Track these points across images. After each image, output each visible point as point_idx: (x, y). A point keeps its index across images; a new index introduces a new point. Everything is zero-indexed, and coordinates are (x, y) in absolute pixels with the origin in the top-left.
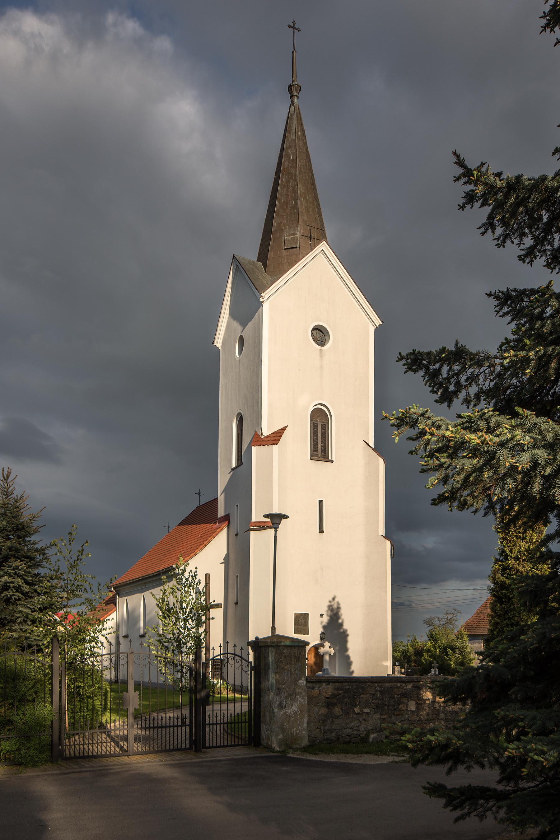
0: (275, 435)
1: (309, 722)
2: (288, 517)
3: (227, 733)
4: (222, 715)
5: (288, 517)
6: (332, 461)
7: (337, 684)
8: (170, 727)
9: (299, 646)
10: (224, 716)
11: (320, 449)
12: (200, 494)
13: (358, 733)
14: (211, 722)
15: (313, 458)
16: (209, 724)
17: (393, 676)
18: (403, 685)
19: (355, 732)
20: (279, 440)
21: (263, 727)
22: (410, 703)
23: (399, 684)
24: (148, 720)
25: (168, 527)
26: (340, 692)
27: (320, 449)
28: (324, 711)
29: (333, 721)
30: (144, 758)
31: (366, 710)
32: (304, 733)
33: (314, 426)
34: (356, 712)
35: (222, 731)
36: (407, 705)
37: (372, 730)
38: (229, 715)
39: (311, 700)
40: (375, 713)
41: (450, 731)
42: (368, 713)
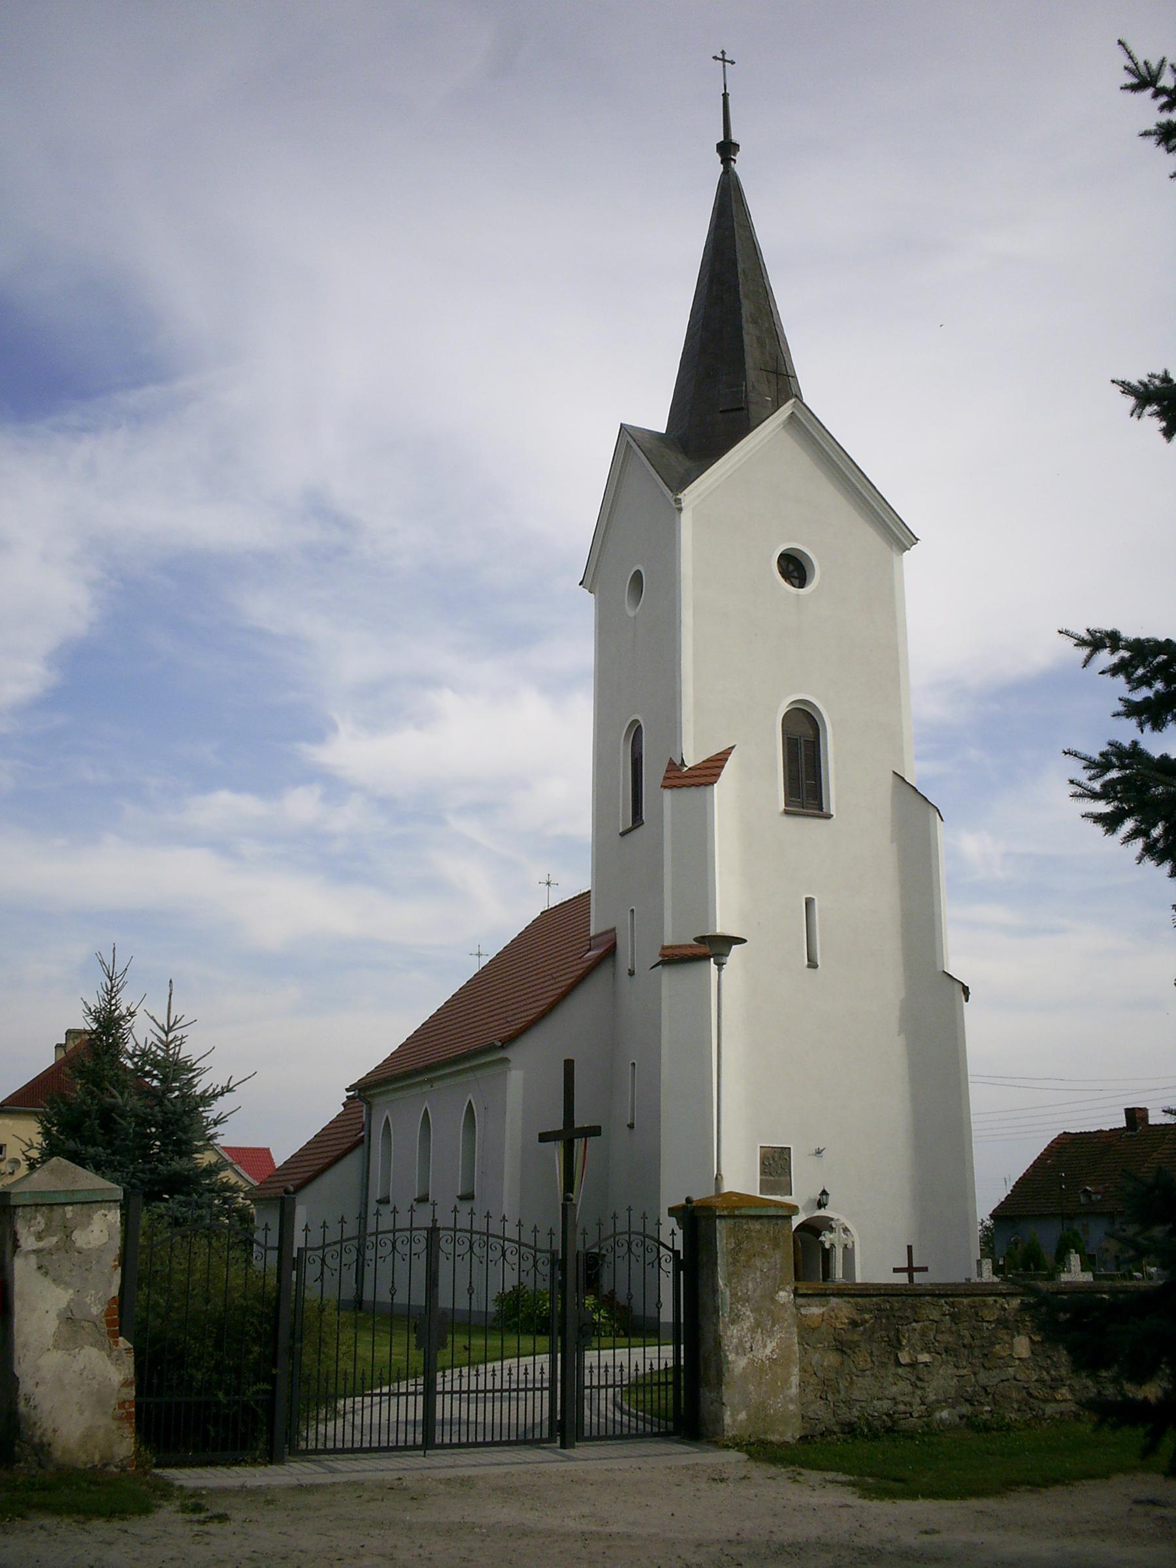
1: (803, 1385)
2: (745, 941)
3: (621, 1409)
4: (359, 1376)
5: (745, 941)
6: (829, 817)
7: (859, 1299)
8: (452, 1392)
9: (778, 1217)
10: (363, 1379)
11: (805, 787)
12: (548, 883)
13: (908, 1409)
15: (669, 782)
16: (444, 1393)
17: (978, 1280)
18: (1001, 1300)
19: (901, 1407)
20: (718, 775)
21: (706, 1395)
22: (1017, 1339)
23: (991, 1299)
24: (498, 1373)
25: (479, 955)
26: (867, 1316)
27: (805, 787)
28: (832, 1359)
30: (209, 1476)
31: (924, 1358)
32: (791, 1407)
33: (791, 745)
34: (903, 1362)
35: (610, 1407)
36: (1012, 1346)
37: (938, 1401)
39: (807, 1332)
40: (945, 1363)
41: (831, 1416)
42: (926, 1364)
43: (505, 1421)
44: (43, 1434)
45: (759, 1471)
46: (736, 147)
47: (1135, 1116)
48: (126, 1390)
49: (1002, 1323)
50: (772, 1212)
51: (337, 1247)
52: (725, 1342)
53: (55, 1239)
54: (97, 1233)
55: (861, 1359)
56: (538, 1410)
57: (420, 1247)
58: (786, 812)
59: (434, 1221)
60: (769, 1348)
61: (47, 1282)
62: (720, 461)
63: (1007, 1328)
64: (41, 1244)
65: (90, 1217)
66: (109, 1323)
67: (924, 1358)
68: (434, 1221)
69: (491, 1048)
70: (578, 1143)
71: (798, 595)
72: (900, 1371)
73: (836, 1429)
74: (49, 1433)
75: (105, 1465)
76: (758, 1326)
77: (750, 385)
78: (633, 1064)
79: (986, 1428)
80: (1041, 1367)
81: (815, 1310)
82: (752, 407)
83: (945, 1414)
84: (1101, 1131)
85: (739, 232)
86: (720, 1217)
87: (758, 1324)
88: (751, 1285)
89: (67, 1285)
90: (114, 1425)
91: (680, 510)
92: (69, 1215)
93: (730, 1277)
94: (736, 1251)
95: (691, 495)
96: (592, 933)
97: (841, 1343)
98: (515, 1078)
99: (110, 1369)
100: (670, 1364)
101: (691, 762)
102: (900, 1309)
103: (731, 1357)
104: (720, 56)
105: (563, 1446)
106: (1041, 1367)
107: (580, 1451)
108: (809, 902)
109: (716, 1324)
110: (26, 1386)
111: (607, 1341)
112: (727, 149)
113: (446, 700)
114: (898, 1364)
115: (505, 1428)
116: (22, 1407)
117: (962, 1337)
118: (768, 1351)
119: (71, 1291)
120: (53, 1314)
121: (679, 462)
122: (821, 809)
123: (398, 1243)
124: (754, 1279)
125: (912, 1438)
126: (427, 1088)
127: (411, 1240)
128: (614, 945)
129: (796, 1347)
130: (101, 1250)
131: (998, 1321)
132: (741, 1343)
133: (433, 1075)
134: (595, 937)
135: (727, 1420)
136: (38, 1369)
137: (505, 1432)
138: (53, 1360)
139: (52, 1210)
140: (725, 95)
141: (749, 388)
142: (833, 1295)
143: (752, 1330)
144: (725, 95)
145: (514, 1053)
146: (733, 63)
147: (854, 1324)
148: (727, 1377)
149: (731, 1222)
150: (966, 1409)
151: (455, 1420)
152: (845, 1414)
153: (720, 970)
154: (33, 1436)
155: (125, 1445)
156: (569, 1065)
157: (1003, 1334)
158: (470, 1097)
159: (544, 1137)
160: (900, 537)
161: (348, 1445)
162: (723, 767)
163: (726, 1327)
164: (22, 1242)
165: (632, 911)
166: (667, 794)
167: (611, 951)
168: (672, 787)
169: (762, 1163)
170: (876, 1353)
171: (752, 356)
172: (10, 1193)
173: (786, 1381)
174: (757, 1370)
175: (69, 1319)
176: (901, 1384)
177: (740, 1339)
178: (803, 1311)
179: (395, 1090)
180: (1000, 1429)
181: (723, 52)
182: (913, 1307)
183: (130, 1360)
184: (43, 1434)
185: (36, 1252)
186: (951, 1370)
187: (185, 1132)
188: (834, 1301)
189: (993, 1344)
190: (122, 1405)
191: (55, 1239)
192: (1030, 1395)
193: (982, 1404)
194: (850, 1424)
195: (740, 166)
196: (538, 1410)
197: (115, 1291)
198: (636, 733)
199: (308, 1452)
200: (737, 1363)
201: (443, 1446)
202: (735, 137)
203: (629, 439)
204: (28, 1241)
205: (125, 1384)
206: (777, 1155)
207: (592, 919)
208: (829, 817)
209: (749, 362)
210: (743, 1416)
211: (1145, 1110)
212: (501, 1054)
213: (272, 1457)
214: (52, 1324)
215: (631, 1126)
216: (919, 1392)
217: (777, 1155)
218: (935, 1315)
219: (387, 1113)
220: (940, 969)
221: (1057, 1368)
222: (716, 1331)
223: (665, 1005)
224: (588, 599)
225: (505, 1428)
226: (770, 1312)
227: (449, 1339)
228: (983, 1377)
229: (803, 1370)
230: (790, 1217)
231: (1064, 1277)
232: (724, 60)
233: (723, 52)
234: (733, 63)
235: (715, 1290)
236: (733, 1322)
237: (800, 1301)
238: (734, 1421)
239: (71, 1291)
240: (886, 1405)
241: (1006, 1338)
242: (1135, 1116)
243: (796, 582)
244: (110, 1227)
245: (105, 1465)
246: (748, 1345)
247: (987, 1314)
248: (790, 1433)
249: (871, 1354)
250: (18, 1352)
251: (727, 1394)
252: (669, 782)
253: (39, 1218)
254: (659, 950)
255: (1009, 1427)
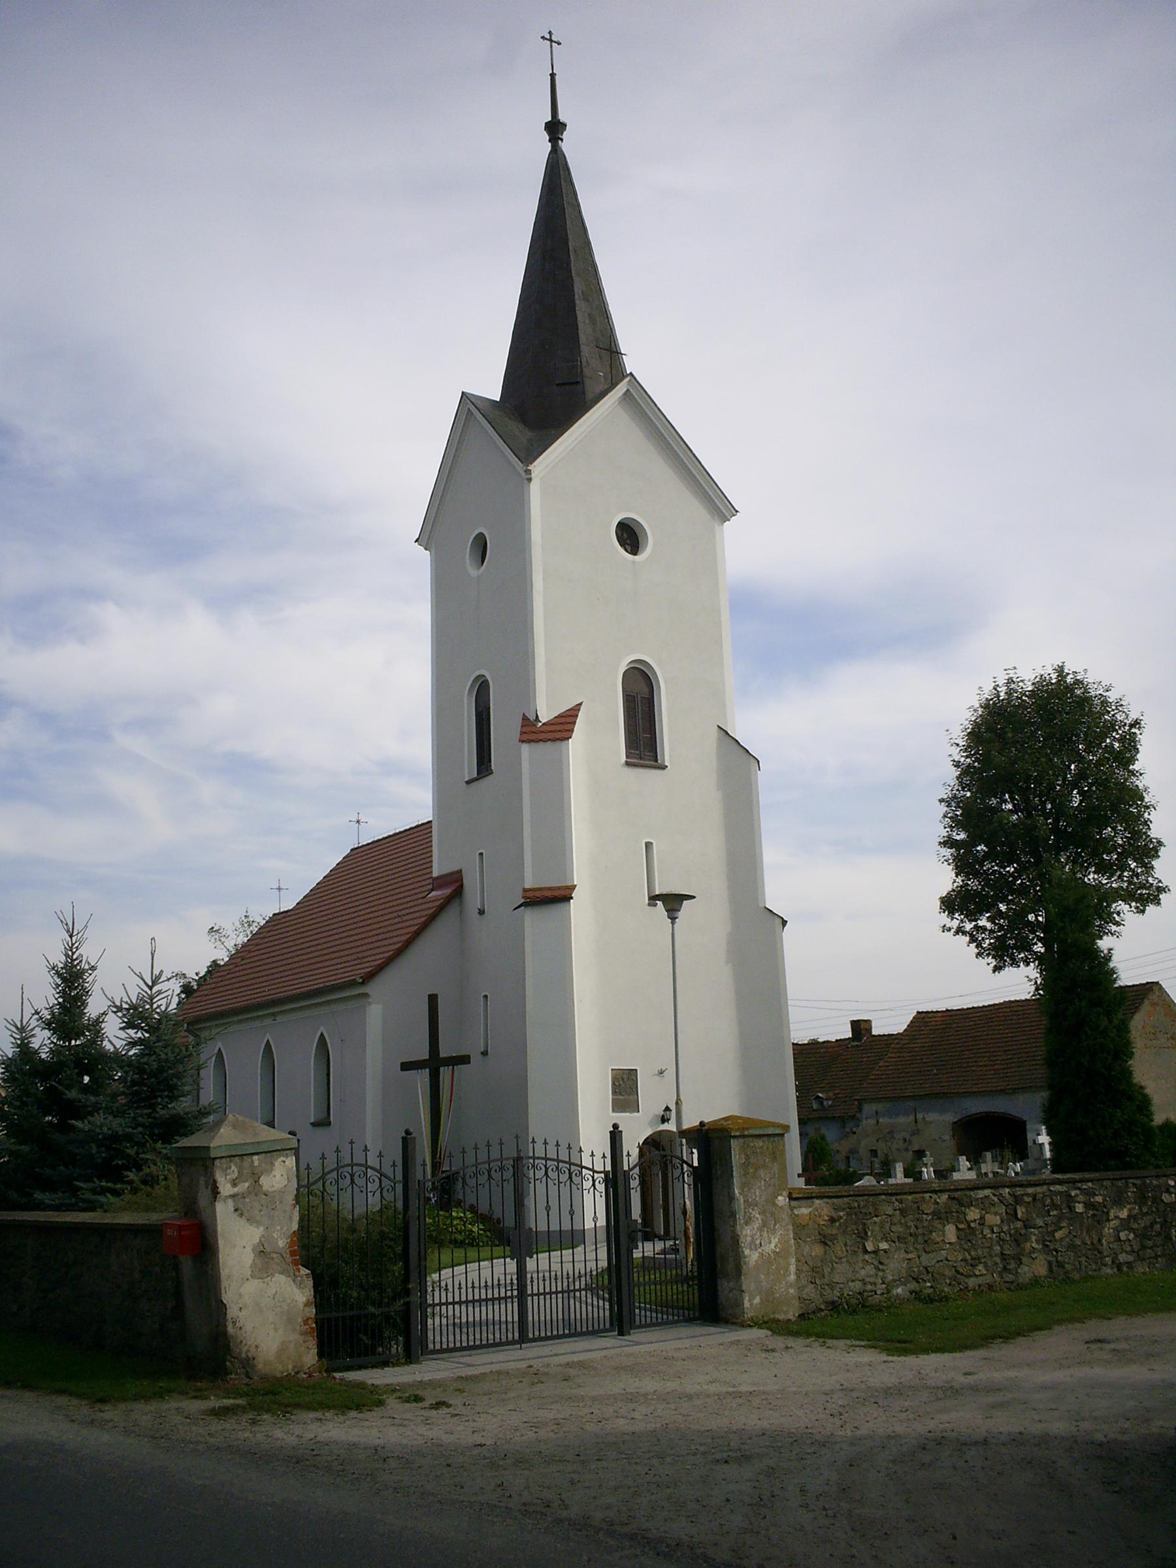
0: (563, 720)
1: (799, 1271)
6: (664, 767)
11: (643, 744)
14: (535, 1291)
15: (526, 737)
16: (532, 1295)
18: (934, 1196)
19: (869, 1287)
21: (724, 1286)
23: (927, 1195)
27: (643, 744)
28: (818, 1250)
29: (833, 1269)
31: (884, 1246)
32: (791, 1291)
33: (630, 701)
37: (894, 1281)
38: (565, 1273)
39: (800, 1229)
42: (885, 1251)
43: (578, 1317)
44: (248, 1351)
45: (779, 1342)
46: (564, 126)
47: (860, 1028)
48: (307, 1309)
49: (936, 1215)
50: (770, 1131)
51: (334, 1174)
52: (742, 1240)
53: (247, 1185)
54: (278, 1177)
55: (839, 1249)
56: (554, 1310)
57: (508, 1174)
58: (627, 764)
59: (519, 1151)
60: (772, 1244)
61: (242, 1222)
62: (565, 435)
63: (939, 1218)
64: (236, 1190)
65: (273, 1164)
66: (292, 1253)
67: (884, 1246)
68: (519, 1151)
69: (352, 984)
70: (445, 1072)
71: (634, 562)
72: (867, 1257)
73: (823, 1307)
74: (253, 1350)
75: (297, 1373)
76: (764, 1226)
77: (584, 360)
78: (486, 997)
79: (930, 1300)
80: (965, 1250)
81: (804, 1211)
82: (587, 382)
83: (899, 1290)
84: (828, 1042)
85: (568, 211)
86: (735, 1137)
87: (764, 1224)
88: (758, 1193)
89: (258, 1223)
90: (301, 1339)
91: (530, 480)
92: (256, 1163)
93: (743, 1186)
94: (745, 1166)
95: (541, 466)
96: (435, 874)
97: (824, 1236)
98: (375, 1013)
99: (294, 1293)
100: (605, 1264)
101: (544, 719)
102: (865, 1206)
103: (747, 1252)
104: (548, 36)
105: (621, 1333)
106: (965, 1250)
107: (636, 1336)
108: (648, 845)
109: (734, 1226)
110: (232, 1312)
111: (486, 1251)
112: (555, 129)
113: (109, 614)
114: (866, 1251)
115: (602, 1320)
116: (230, 1329)
117: (909, 1228)
118: (772, 1246)
119: (262, 1228)
120: (249, 1249)
121: (523, 434)
122: (656, 761)
123: (493, 1172)
124: (760, 1188)
125: (880, 1310)
126: (268, 1021)
127: (502, 1168)
128: (462, 886)
129: (793, 1241)
130: (282, 1192)
131: (933, 1213)
132: (753, 1241)
133: (276, 1010)
134: (437, 878)
135: (747, 1304)
136: (240, 1295)
137: (584, 1325)
138: (252, 1287)
139: (242, 1160)
140: (553, 76)
141: (584, 364)
142: (817, 1198)
143: (760, 1229)
144: (553, 76)
145: (372, 988)
146: (559, 44)
147: (833, 1220)
148: (745, 1269)
149: (741, 1140)
150: (913, 1285)
151: (490, 1321)
152: (834, 1295)
153: (673, 923)
154: (240, 1353)
155: (310, 1357)
156: (433, 1000)
157: (936, 1223)
158: (322, 1029)
159: (406, 1066)
160: (720, 508)
161: (438, 1347)
162: (574, 723)
163: (742, 1228)
164: (221, 1189)
165: (481, 854)
166: (525, 748)
167: (459, 892)
168: (529, 741)
169: (613, 1084)
170: (849, 1243)
171: (585, 332)
172: (209, 1148)
173: (787, 1270)
174: (766, 1260)
175: (261, 1252)
176: (868, 1268)
177: (752, 1236)
178: (796, 1212)
179: (240, 1021)
180: (941, 1300)
181: (550, 33)
182: (874, 1205)
183: (310, 1283)
184: (248, 1351)
185: (233, 1196)
186: (903, 1255)
187: (179, 1079)
188: (817, 1202)
189: (931, 1232)
190: (306, 1322)
191: (247, 1185)
192: (958, 1272)
193: (925, 1281)
194: (833, 1302)
195: (567, 145)
196: (554, 1310)
197: (295, 1227)
198: (482, 689)
199: (435, 1352)
200: (752, 1257)
201: (534, 1340)
202: (562, 117)
203: (473, 408)
204: (226, 1189)
205: (307, 1304)
206: (625, 1077)
207: (435, 859)
208: (664, 767)
209: (583, 338)
210: (757, 1300)
211: (868, 1022)
212: (361, 990)
213: (409, 1357)
214: (248, 1258)
215: (485, 1053)
216: (880, 1274)
217: (625, 1077)
218: (890, 1211)
219: (220, 1045)
220: (761, 905)
221: (976, 1250)
222: (734, 1232)
223: (528, 944)
224: (424, 556)
225: (602, 1320)
226: (772, 1214)
227: (640, 1245)
228: (926, 1260)
229: (798, 1260)
230: (782, 1135)
231: (956, 1176)
232: (551, 40)
233: (550, 33)
234: (559, 44)
235: (731, 1198)
236: (747, 1223)
237: (794, 1203)
238: (752, 1304)
239: (262, 1228)
240: (857, 1286)
241: (940, 1227)
242: (860, 1028)
243: (629, 548)
244: (289, 1170)
245: (297, 1373)
246: (758, 1242)
247: (924, 1207)
248: (791, 1313)
249: (846, 1245)
250: (224, 1283)
251: (747, 1283)
252: (526, 737)
253: (233, 1168)
254: (520, 893)
255: (947, 1299)
